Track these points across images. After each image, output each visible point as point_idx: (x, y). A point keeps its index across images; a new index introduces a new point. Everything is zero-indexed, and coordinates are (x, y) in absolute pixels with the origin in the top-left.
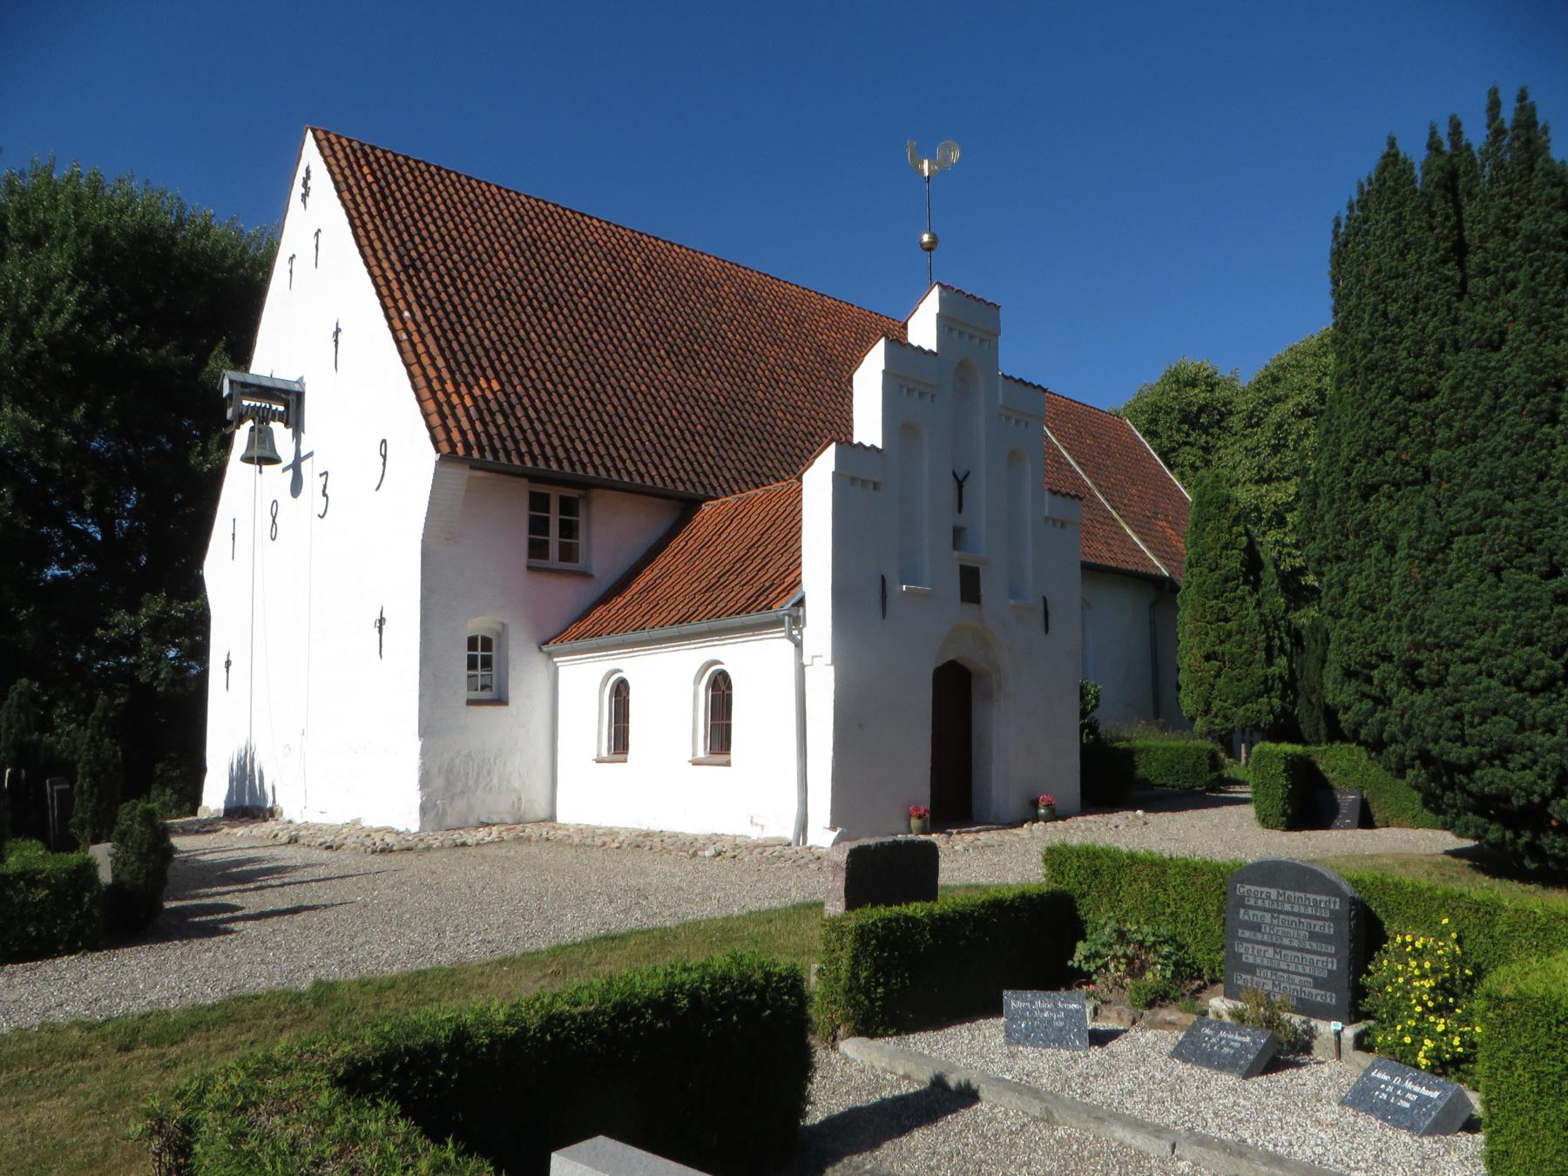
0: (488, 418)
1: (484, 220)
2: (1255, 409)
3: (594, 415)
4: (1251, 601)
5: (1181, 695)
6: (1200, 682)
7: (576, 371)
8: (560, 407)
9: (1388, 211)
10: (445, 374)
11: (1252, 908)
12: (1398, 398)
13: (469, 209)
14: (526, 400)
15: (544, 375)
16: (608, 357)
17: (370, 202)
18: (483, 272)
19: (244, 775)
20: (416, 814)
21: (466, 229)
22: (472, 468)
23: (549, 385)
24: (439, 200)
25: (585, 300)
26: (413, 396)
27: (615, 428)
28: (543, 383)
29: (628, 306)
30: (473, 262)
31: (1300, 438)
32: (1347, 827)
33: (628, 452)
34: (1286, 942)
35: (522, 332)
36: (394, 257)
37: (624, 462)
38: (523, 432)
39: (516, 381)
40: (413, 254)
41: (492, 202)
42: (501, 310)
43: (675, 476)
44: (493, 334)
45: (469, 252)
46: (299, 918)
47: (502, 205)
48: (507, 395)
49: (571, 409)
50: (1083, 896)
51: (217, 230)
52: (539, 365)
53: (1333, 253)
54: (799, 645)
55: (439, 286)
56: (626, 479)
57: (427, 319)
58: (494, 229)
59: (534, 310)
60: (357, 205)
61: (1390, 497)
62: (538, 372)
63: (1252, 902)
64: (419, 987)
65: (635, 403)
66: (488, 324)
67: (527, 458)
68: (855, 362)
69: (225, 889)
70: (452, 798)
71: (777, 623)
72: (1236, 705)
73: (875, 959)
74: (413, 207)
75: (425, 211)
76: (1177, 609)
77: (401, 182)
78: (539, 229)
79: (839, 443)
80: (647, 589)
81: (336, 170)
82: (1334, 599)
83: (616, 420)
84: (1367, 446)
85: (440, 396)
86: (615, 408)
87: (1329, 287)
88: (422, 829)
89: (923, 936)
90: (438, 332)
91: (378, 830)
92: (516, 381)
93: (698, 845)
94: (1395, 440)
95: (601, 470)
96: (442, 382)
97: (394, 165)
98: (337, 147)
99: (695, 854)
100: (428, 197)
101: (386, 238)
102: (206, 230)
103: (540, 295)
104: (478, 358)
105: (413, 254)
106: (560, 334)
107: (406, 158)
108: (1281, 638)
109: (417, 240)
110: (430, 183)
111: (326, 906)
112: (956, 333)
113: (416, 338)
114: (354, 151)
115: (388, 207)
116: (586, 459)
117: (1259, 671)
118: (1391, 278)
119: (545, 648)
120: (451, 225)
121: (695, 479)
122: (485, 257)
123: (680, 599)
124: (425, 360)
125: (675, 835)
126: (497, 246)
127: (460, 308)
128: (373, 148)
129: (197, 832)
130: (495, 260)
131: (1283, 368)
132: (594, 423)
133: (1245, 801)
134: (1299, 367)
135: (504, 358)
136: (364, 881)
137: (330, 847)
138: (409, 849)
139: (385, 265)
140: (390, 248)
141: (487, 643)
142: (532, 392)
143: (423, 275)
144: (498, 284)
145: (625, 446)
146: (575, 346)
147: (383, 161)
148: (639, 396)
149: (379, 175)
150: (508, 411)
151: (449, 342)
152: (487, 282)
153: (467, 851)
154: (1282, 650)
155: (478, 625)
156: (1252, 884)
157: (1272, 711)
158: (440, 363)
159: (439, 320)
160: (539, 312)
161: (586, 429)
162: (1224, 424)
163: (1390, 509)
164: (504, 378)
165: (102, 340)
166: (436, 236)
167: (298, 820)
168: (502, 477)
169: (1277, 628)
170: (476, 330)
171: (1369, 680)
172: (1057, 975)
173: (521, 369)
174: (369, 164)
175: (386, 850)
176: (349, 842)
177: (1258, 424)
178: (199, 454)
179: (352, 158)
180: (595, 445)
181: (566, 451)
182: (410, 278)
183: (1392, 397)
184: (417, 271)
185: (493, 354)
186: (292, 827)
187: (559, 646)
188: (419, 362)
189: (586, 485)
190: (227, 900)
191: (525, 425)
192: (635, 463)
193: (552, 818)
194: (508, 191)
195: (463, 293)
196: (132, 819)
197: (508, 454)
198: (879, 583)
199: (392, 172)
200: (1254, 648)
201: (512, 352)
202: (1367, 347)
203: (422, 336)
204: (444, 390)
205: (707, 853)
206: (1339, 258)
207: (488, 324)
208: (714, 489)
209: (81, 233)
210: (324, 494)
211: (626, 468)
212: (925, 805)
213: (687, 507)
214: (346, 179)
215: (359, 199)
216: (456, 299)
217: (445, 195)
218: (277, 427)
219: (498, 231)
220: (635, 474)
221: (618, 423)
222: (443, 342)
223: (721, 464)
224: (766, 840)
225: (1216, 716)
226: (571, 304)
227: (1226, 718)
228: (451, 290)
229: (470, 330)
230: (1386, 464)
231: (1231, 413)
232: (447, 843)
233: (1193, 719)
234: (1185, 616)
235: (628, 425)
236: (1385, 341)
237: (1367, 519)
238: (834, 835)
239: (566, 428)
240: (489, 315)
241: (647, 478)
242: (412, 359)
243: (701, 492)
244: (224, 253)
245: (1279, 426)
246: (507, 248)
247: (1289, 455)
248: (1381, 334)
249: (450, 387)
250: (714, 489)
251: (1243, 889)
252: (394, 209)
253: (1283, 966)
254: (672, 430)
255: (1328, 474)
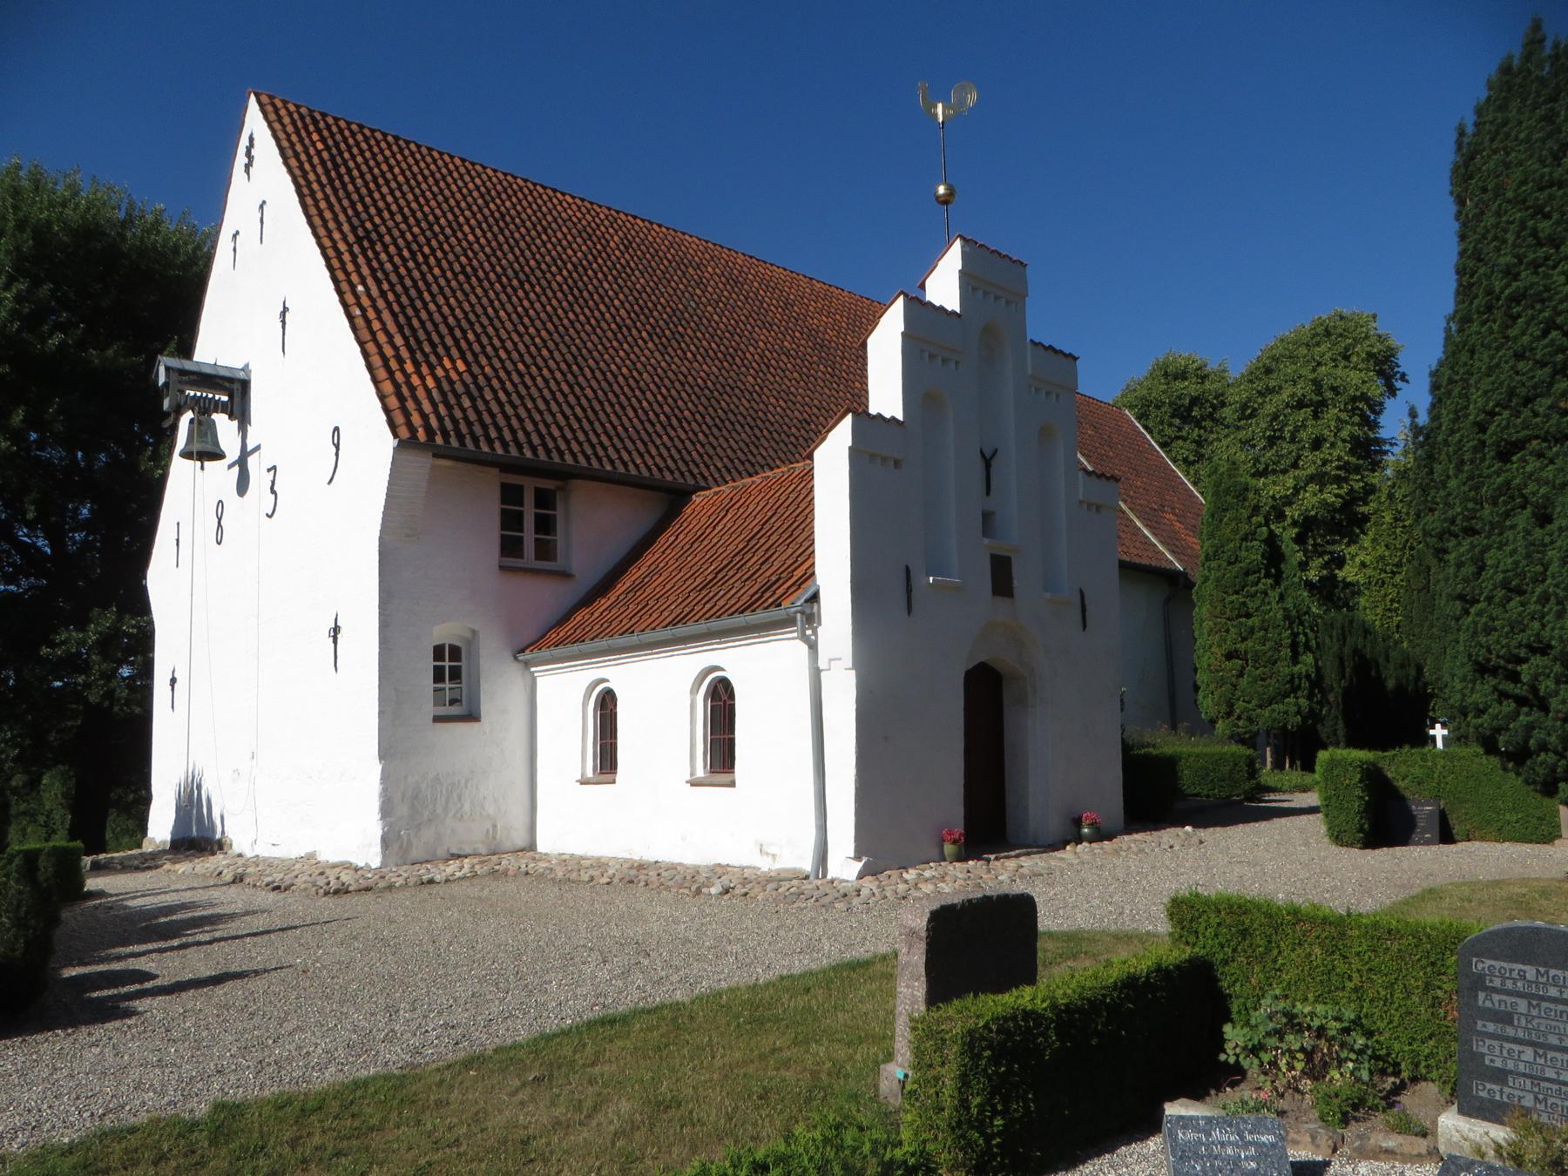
0: (453, 401)
1: (447, 192)
2: (1249, 400)
3: (571, 399)
4: (1274, 595)
5: (1200, 697)
6: (1221, 682)
7: (551, 352)
8: (533, 390)
9: (1536, 106)
10: (405, 353)
11: (1495, 990)
12: (1554, 334)
13: (431, 181)
14: (495, 382)
15: (515, 355)
16: (585, 337)
17: (320, 170)
18: (446, 246)
19: (191, 804)
20: (377, 848)
21: (427, 201)
22: (435, 456)
23: (521, 366)
24: (397, 170)
25: (559, 278)
26: (368, 376)
27: (596, 413)
28: (515, 364)
29: (606, 285)
30: (436, 236)
31: (1297, 429)
32: (1428, 843)
33: (610, 438)
34: (1553, 1040)
35: (490, 310)
36: (346, 228)
37: (605, 449)
38: (493, 416)
39: (484, 361)
40: (368, 225)
41: (455, 175)
42: (466, 286)
43: (662, 465)
44: (458, 311)
45: (431, 226)
46: (220, 991)
47: (467, 178)
48: (474, 377)
49: (546, 392)
50: (1225, 962)
51: (169, 226)
52: (509, 345)
53: (1455, 170)
54: (813, 647)
55: (397, 259)
56: (609, 468)
57: (383, 294)
58: (458, 203)
59: (504, 287)
60: (305, 174)
61: (1540, 455)
62: (508, 352)
63: (1497, 983)
64: (355, 1109)
65: (615, 387)
66: (452, 300)
67: (497, 445)
68: (873, 322)
69: (144, 947)
70: (418, 827)
71: (789, 622)
72: (1260, 707)
73: (989, 1078)
74: (368, 177)
75: (381, 181)
76: (1194, 606)
77: (355, 151)
78: (508, 204)
79: (856, 415)
80: (634, 589)
81: (282, 136)
82: (1466, 580)
83: (595, 404)
84: (1511, 393)
85: (399, 377)
86: (594, 392)
87: (1453, 208)
88: (384, 864)
89: (1047, 1038)
90: (396, 308)
91: (334, 866)
92: (484, 361)
93: (701, 879)
94: (1551, 384)
95: (581, 458)
96: (401, 361)
97: (347, 133)
98: (283, 112)
99: (698, 892)
100: (384, 167)
101: (337, 208)
102: (157, 223)
103: (510, 272)
104: (442, 337)
105: (368, 225)
106: (531, 312)
107: (361, 127)
108: (1305, 635)
109: (373, 211)
110: (387, 153)
111: (256, 973)
112: (980, 294)
113: (371, 314)
114: (302, 117)
115: (340, 176)
116: (563, 446)
117: (1284, 669)
118: (1541, 189)
119: (521, 657)
120: (410, 197)
121: (684, 469)
122: (448, 231)
123: (672, 598)
124: (382, 338)
125: (672, 867)
126: (461, 219)
127: (421, 284)
128: (324, 115)
129: (137, 869)
130: (459, 235)
131: (1275, 359)
132: (572, 408)
133: (1312, 810)
134: (1292, 358)
135: (471, 336)
136: (308, 935)
137: (278, 888)
138: (368, 889)
139: (337, 236)
140: (342, 218)
141: (455, 653)
142: (502, 374)
143: (378, 247)
144: (463, 259)
145: (606, 433)
146: (549, 325)
147: (334, 129)
148: (620, 379)
149: (330, 142)
150: (476, 394)
151: (408, 319)
152: (451, 257)
153: (435, 889)
154: (1307, 647)
155: (446, 632)
156: (1496, 959)
157: (1299, 712)
158: (399, 341)
159: (397, 297)
160: (509, 290)
161: (562, 412)
162: (1217, 416)
163: (1542, 469)
164: (470, 358)
165: (43, 341)
166: (394, 208)
167: (249, 854)
168: (470, 466)
169: (1301, 623)
170: (439, 307)
171: (1514, 677)
172: (1206, 1074)
173: (489, 349)
174: (319, 131)
175: (342, 891)
176: (299, 881)
177: (1251, 416)
178: (150, 459)
179: (299, 124)
180: (573, 431)
181: (541, 436)
182: (364, 251)
183: (1545, 333)
184: (372, 244)
185: (458, 333)
186: (240, 862)
187: (536, 654)
188: (375, 340)
189: (566, 475)
190: (132, 964)
191: (495, 408)
192: (618, 451)
193: (532, 847)
194: (473, 164)
195: (424, 268)
196: (7, 875)
197: (476, 440)
198: (904, 575)
199: (345, 140)
200: (1279, 644)
201: (479, 330)
202: (1511, 274)
203: (378, 312)
204: (403, 371)
205: (713, 891)
206: (1465, 174)
207: (452, 300)
208: (705, 478)
209: (21, 225)
210: (273, 491)
211: (608, 456)
212: (959, 829)
213: (675, 499)
214: (292, 145)
215: (307, 167)
216: (416, 274)
217: (404, 165)
218: (220, 419)
219: (463, 204)
220: (618, 463)
221: (598, 408)
222: (402, 319)
223: (711, 452)
224: (779, 872)
225: (1239, 718)
226: (543, 282)
227: (1250, 720)
228: (411, 264)
229: (432, 307)
230: (1536, 415)
231: (1223, 404)
232: (412, 881)
233: (1213, 722)
234: (1202, 611)
235: (609, 409)
236: (1535, 265)
237: (1508, 483)
238: (859, 865)
239: (541, 413)
240: (454, 292)
241: (631, 467)
242: (367, 336)
243: (692, 482)
244: (176, 250)
245: (1275, 417)
246: (473, 222)
247: (1286, 447)
248: (1531, 256)
249: (409, 367)
250: (705, 478)
251: (1481, 965)
252: (346, 179)
253: (1550, 1074)
254: (657, 416)
255: (1452, 432)
